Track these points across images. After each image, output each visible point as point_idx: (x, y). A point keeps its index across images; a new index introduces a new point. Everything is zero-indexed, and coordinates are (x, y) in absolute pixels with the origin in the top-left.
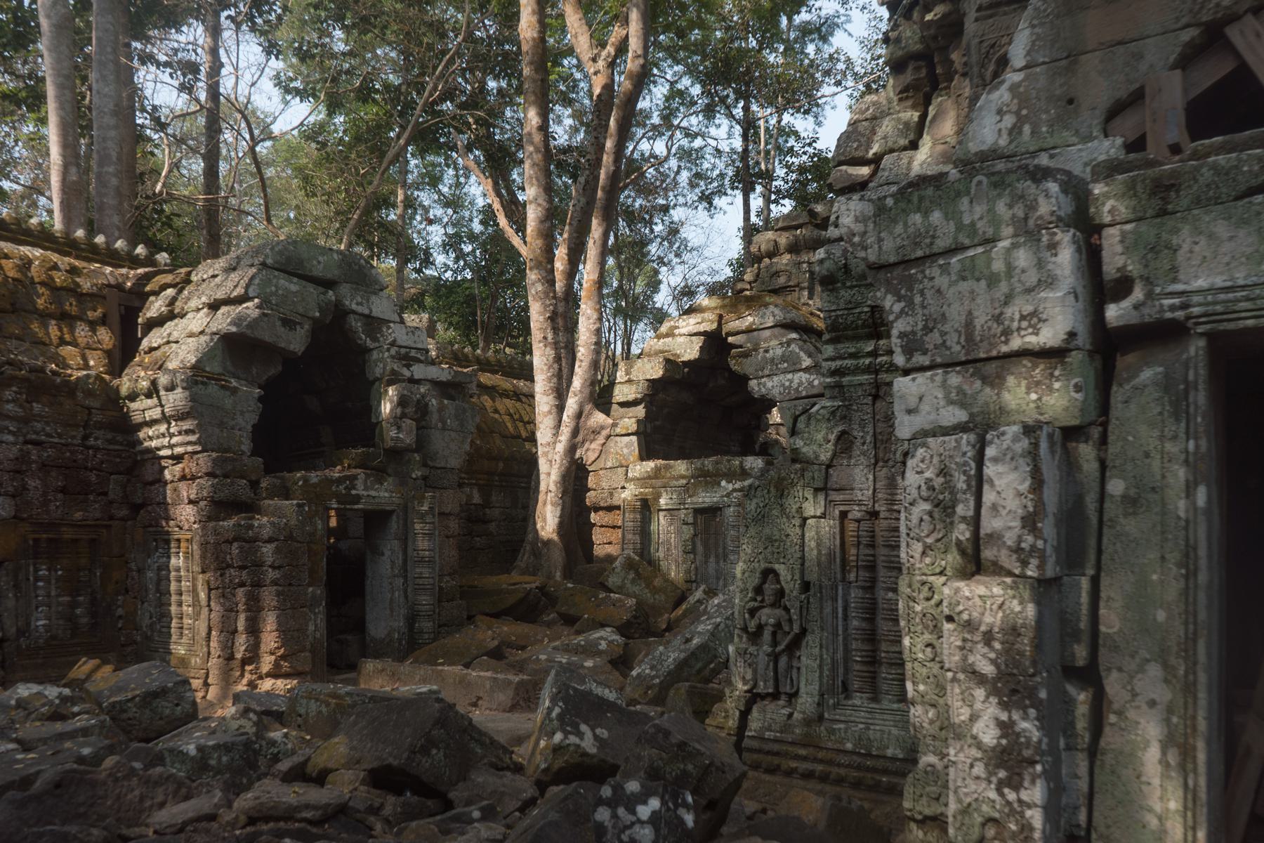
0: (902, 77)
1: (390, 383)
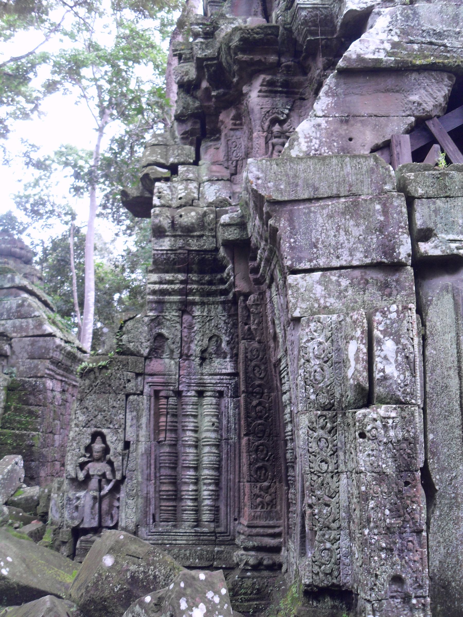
0: (184, 126)
1: (249, 79)
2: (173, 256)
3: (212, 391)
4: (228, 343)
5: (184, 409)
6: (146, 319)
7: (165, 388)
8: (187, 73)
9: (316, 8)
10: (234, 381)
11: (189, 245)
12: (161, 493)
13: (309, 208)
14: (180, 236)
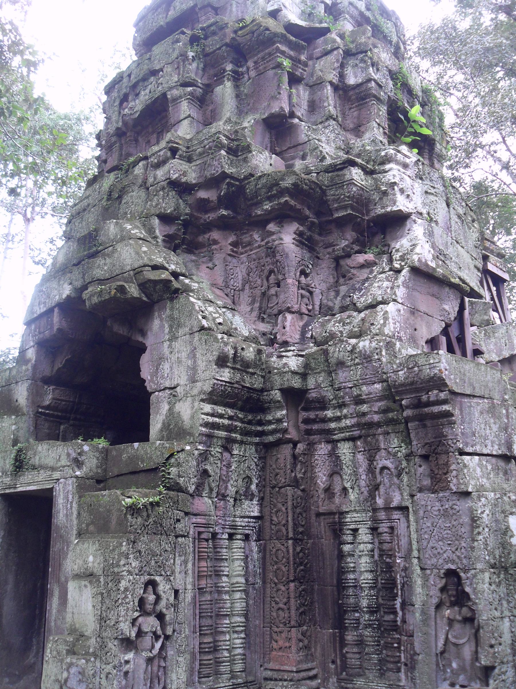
0: (168, 228)
2: (229, 389)
3: (241, 534)
4: (257, 485)
5: (219, 552)
6: (196, 453)
7: (206, 530)
8: (185, 174)
9: (363, 189)
10: (257, 524)
11: (244, 380)
12: (203, 646)
13: (470, 402)
14: (238, 369)
